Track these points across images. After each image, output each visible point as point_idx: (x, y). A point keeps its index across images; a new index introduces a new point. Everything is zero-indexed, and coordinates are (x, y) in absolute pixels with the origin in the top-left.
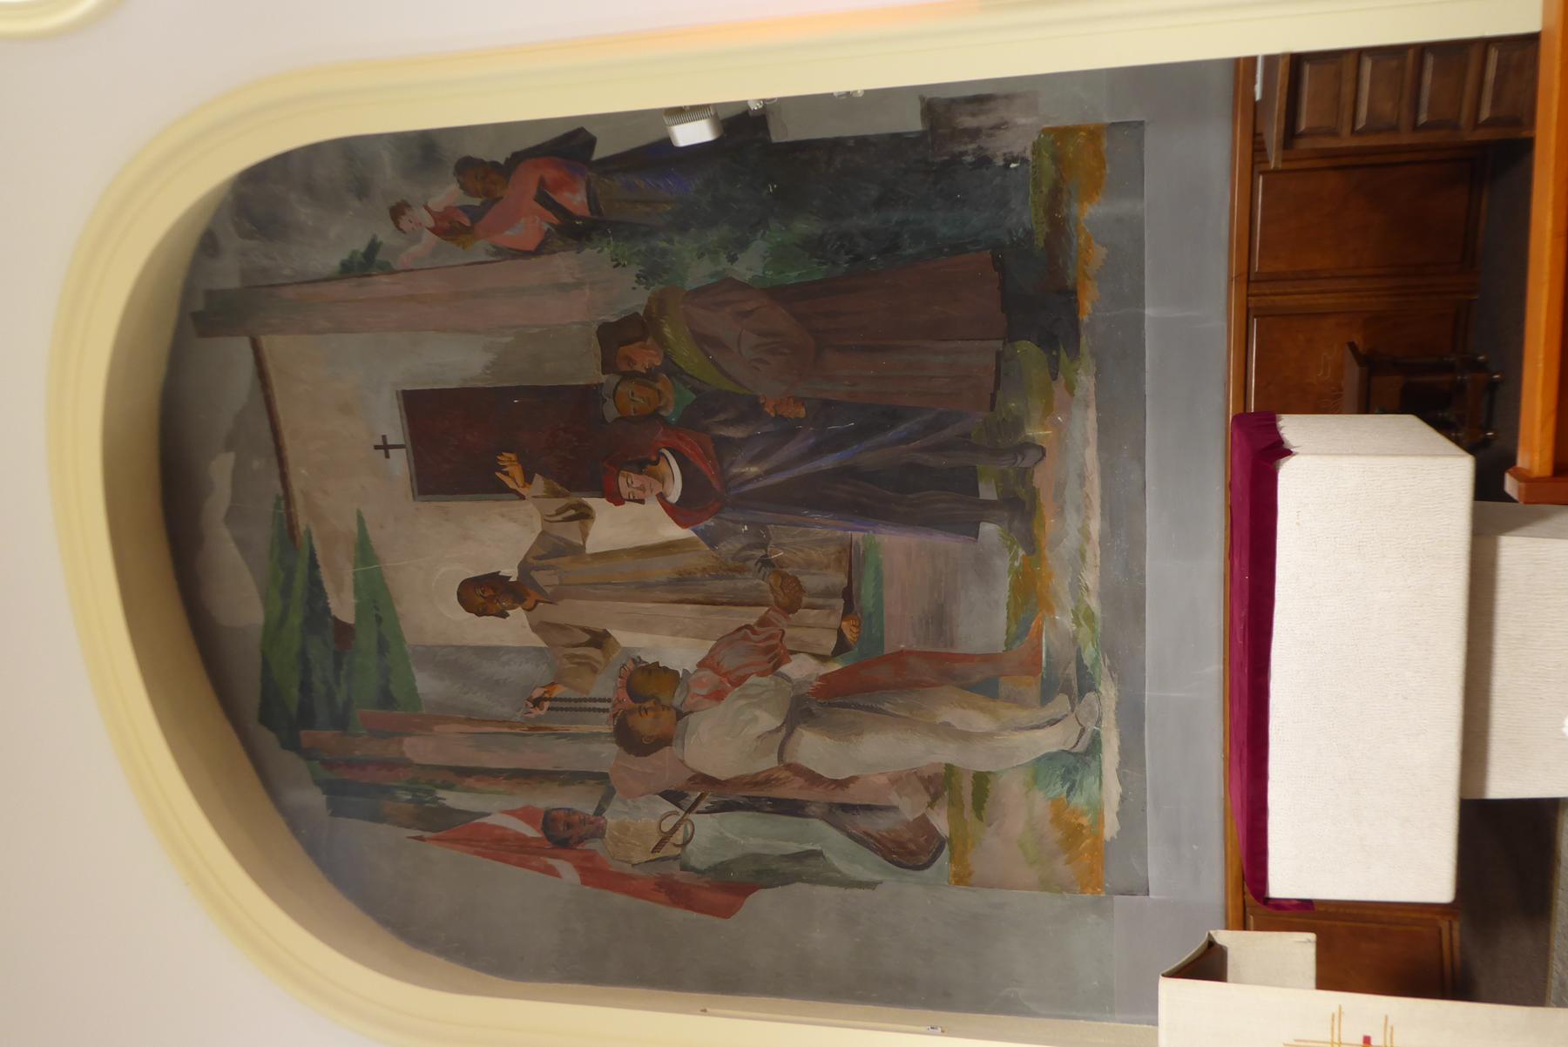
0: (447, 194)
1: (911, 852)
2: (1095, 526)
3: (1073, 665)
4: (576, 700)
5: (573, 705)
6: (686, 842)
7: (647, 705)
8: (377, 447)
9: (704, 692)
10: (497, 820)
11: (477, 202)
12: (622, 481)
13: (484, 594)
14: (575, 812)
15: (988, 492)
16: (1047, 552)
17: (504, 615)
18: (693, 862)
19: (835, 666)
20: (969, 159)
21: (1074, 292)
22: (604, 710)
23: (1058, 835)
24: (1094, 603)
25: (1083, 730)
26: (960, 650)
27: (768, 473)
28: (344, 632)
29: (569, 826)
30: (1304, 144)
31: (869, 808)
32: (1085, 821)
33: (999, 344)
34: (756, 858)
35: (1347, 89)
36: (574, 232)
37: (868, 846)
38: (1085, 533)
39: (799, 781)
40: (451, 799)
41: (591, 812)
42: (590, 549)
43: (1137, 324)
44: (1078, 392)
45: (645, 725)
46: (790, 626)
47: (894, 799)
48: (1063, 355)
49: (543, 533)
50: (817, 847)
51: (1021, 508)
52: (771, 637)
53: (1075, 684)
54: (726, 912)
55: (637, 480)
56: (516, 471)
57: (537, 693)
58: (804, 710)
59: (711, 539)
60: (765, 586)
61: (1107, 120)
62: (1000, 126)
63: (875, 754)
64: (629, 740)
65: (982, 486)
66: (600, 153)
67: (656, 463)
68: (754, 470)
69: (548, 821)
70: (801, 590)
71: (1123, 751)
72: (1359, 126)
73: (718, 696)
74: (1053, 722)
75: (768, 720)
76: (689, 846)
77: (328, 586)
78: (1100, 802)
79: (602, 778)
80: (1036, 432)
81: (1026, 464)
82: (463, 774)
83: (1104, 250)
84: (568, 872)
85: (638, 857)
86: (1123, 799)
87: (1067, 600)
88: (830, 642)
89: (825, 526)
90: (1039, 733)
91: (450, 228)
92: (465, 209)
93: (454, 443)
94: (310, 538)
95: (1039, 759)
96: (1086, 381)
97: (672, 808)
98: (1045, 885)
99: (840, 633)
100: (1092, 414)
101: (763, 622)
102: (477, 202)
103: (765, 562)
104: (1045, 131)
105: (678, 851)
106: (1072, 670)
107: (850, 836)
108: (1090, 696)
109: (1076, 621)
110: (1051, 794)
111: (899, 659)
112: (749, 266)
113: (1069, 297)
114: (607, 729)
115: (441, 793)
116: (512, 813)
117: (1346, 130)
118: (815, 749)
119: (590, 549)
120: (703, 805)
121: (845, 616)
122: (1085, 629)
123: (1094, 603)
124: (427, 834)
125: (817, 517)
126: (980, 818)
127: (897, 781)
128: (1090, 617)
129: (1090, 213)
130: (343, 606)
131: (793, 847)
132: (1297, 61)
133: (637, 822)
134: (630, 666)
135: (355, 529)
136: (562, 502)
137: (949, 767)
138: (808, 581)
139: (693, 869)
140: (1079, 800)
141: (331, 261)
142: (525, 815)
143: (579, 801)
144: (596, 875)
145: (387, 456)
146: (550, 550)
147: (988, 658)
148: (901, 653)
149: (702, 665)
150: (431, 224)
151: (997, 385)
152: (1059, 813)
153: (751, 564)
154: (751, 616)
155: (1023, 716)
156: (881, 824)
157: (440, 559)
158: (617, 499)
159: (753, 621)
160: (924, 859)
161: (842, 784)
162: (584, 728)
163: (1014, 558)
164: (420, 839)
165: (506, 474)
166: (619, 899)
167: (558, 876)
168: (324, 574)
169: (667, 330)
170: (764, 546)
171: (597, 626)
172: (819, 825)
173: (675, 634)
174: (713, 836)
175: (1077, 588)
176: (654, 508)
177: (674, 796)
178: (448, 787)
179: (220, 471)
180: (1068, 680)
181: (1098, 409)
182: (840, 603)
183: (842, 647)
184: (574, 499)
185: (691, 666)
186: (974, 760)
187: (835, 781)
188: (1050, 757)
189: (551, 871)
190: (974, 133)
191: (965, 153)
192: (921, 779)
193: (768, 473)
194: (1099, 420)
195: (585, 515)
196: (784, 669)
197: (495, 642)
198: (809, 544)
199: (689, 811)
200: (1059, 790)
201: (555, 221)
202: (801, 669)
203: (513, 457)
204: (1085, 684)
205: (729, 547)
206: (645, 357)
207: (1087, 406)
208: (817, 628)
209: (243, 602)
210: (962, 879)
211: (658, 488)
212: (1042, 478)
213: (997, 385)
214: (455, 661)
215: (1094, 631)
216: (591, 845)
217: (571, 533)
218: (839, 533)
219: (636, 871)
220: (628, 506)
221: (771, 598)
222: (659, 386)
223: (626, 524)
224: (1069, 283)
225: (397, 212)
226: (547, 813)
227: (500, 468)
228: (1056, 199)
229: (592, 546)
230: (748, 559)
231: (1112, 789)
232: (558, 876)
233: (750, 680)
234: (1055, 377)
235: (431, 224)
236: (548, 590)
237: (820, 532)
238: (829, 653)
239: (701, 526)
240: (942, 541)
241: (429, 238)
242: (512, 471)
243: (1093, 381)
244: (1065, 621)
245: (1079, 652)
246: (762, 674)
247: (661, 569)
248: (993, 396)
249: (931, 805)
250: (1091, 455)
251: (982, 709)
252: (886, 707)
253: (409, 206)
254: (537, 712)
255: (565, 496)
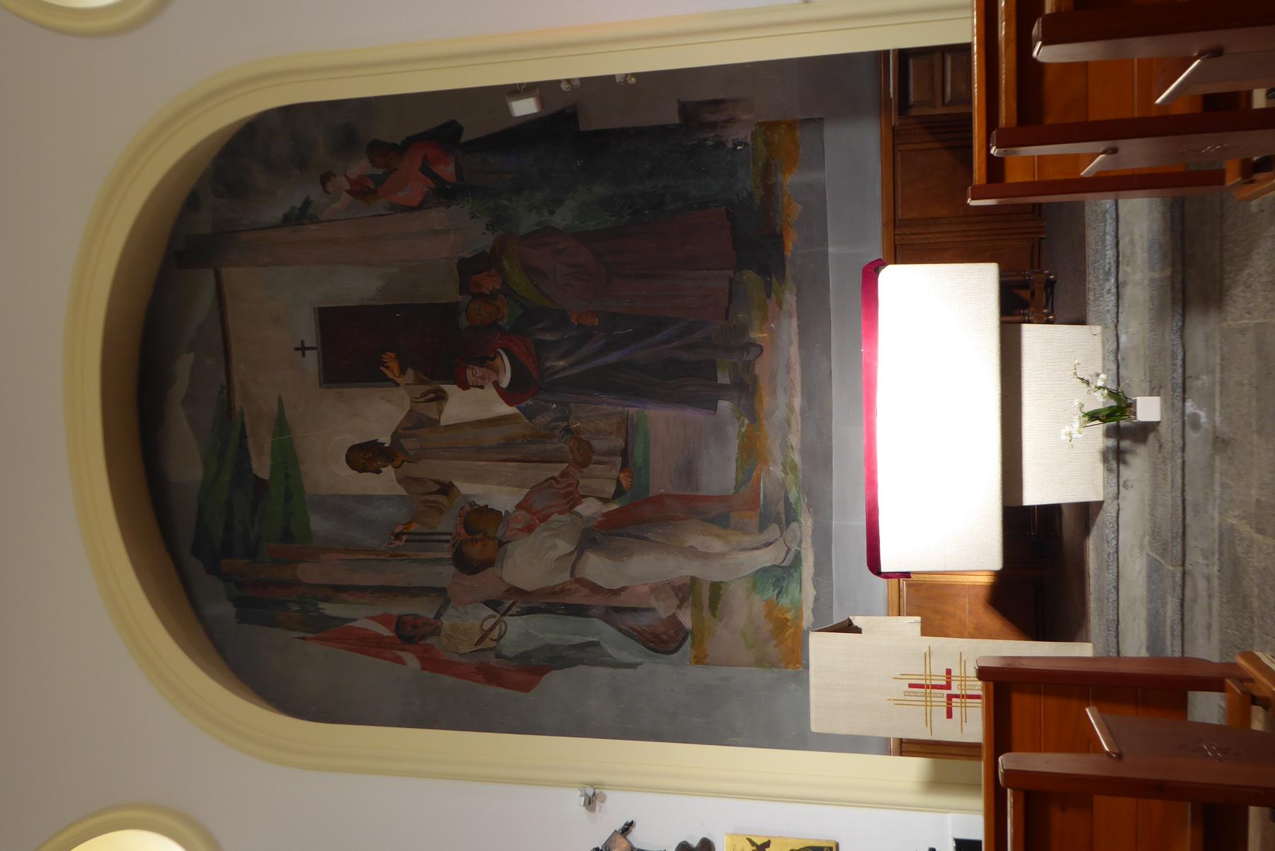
0: (360, 167)
1: (664, 641)
2: (797, 402)
3: (782, 503)
4: (426, 534)
5: (424, 537)
6: (500, 638)
7: (477, 537)
8: (297, 349)
9: (519, 526)
10: (363, 624)
11: (380, 172)
12: (469, 372)
13: (365, 456)
14: (420, 617)
15: (723, 378)
16: (764, 422)
17: (378, 472)
18: (505, 652)
19: (614, 506)
20: (710, 143)
21: (781, 236)
22: (447, 541)
23: (770, 626)
24: (796, 457)
25: (789, 550)
26: (704, 493)
27: (571, 366)
28: (261, 485)
29: (414, 627)
30: (914, 112)
31: (635, 610)
32: (789, 616)
33: (731, 273)
34: (551, 647)
35: (938, 75)
36: (444, 193)
37: (632, 637)
38: (790, 407)
39: (585, 591)
40: (329, 609)
41: (431, 616)
42: (443, 423)
43: (825, 255)
44: (785, 306)
45: (475, 551)
46: (584, 477)
47: (653, 603)
48: (774, 280)
49: (411, 411)
50: (595, 639)
51: (746, 389)
52: (570, 485)
53: (783, 516)
54: (527, 687)
55: (479, 371)
56: (394, 365)
57: (398, 530)
58: (596, 537)
59: (529, 414)
60: (567, 448)
61: (799, 117)
62: (731, 121)
63: (641, 570)
64: (466, 564)
65: (719, 374)
66: (465, 138)
67: (493, 359)
68: (562, 363)
69: (400, 624)
70: (591, 450)
71: (816, 564)
72: (947, 100)
73: (529, 529)
74: (768, 545)
75: (564, 547)
76: (503, 640)
77: (252, 452)
78: (800, 602)
79: (442, 591)
80: (757, 335)
81: (749, 359)
82: (337, 591)
83: (800, 207)
84: (412, 661)
85: (464, 649)
86: (816, 600)
87: (777, 454)
88: (611, 489)
89: (609, 404)
90: (757, 553)
91: (361, 191)
92: (371, 177)
93: (353, 347)
94: (243, 416)
95: (757, 572)
96: (790, 299)
97: (491, 612)
98: (761, 662)
99: (618, 481)
100: (794, 322)
101: (564, 474)
102: (380, 172)
103: (567, 430)
104: (758, 124)
105: (494, 644)
106: (781, 507)
107: (620, 630)
108: (794, 525)
109: (784, 470)
110: (766, 597)
111: (659, 500)
112: (563, 218)
113: (777, 240)
114: (448, 555)
115: (322, 605)
116: (372, 618)
117: (939, 102)
118: (597, 568)
119: (443, 423)
120: (514, 610)
121: (622, 470)
122: (791, 476)
123: (796, 457)
124: (309, 635)
125: (605, 397)
126: (714, 615)
127: (656, 590)
128: (794, 468)
129: (791, 180)
130: (262, 467)
131: (579, 640)
132: (904, 55)
133: (466, 621)
134: (468, 508)
135: (276, 408)
136: (425, 388)
137: (693, 579)
138: (596, 444)
139: (505, 657)
140: (785, 601)
141: (274, 213)
142: (383, 620)
143: (423, 609)
144: (432, 662)
145: (304, 355)
146: (416, 423)
147: (722, 499)
148: (661, 496)
149: (518, 507)
150: (348, 187)
151: (730, 302)
152: (771, 608)
153: (557, 432)
154: (555, 470)
155: (747, 540)
156: (644, 621)
157: (336, 433)
158: (465, 386)
159: (556, 474)
160: (673, 646)
161: (616, 593)
162: (431, 555)
163: (741, 426)
164: (303, 638)
165: (387, 367)
166: (448, 680)
167: (404, 664)
168: (250, 441)
169: (505, 264)
170: (566, 418)
171: (445, 479)
172: (598, 624)
173: (500, 484)
174: (520, 632)
175: (785, 446)
176: (490, 392)
177: (493, 604)
178: (327, 600)
179: (184, 365)
180: (779, 514)
181: (799, 319)
182: (618, 460)
183: (619, 492)
184: (434, 386)
185: (511, 508)
186: (709, 573)
187: (611, 591)
188: (765, 570)
189: (399, 660)
190: (713, 125)
191: (707, 139)
192: (673, 588)
193: (571, 366)
194: (799, 327)
195: (441, 397)
196: (579, 509)
197: (370, 492)
198: (597, 417)
199: (504, 614)
200: (771, 593)
201: (433, 185)
202: (590, 508)
203: (392, 355)
204: (791, 516)
205: (542, 419)
206: (490, 283)
207: (791, 317)
208: (602, 478)
209: (188, 463)
210: (700, 660)
211: (494, 378)
212: (760, 368)
213: (730, 302)
214: (341, 506)
215: (796, 477)
216: (431, 641)
217: (430, 410)
218: (620, 409)
219: (463, 660)
220: (473, 391)
221: (571, 456)
222: (498, 303)
223: (473, 404)
224: (778, 229)
225: (325, 179)
226: (400, 618)
227: (383, 364)
228: (767, 171)
229: (444, 420)
230: (555, 428)
231: (809, 592)
232: (404, 664)
233: (552, 518)
234: (769, 296)
235: (348, 187)
236: (412, 453)
237: (606, 408)
238: (610, 497)
239: (523, 405)
240: (691, 414)
241: (346, 198)
242: (391, 365)
243: (795, 298)
244: (777, 470)
245: (786, 493)
246: (561, 513)
247: (493, 436)
248: (727, 310)
249: (679, 607)
250: (794, 351)
251: (717, 536)
252: (650, 535)
253: (333, 175)
254: (398, 543)
255: (428, 383)
